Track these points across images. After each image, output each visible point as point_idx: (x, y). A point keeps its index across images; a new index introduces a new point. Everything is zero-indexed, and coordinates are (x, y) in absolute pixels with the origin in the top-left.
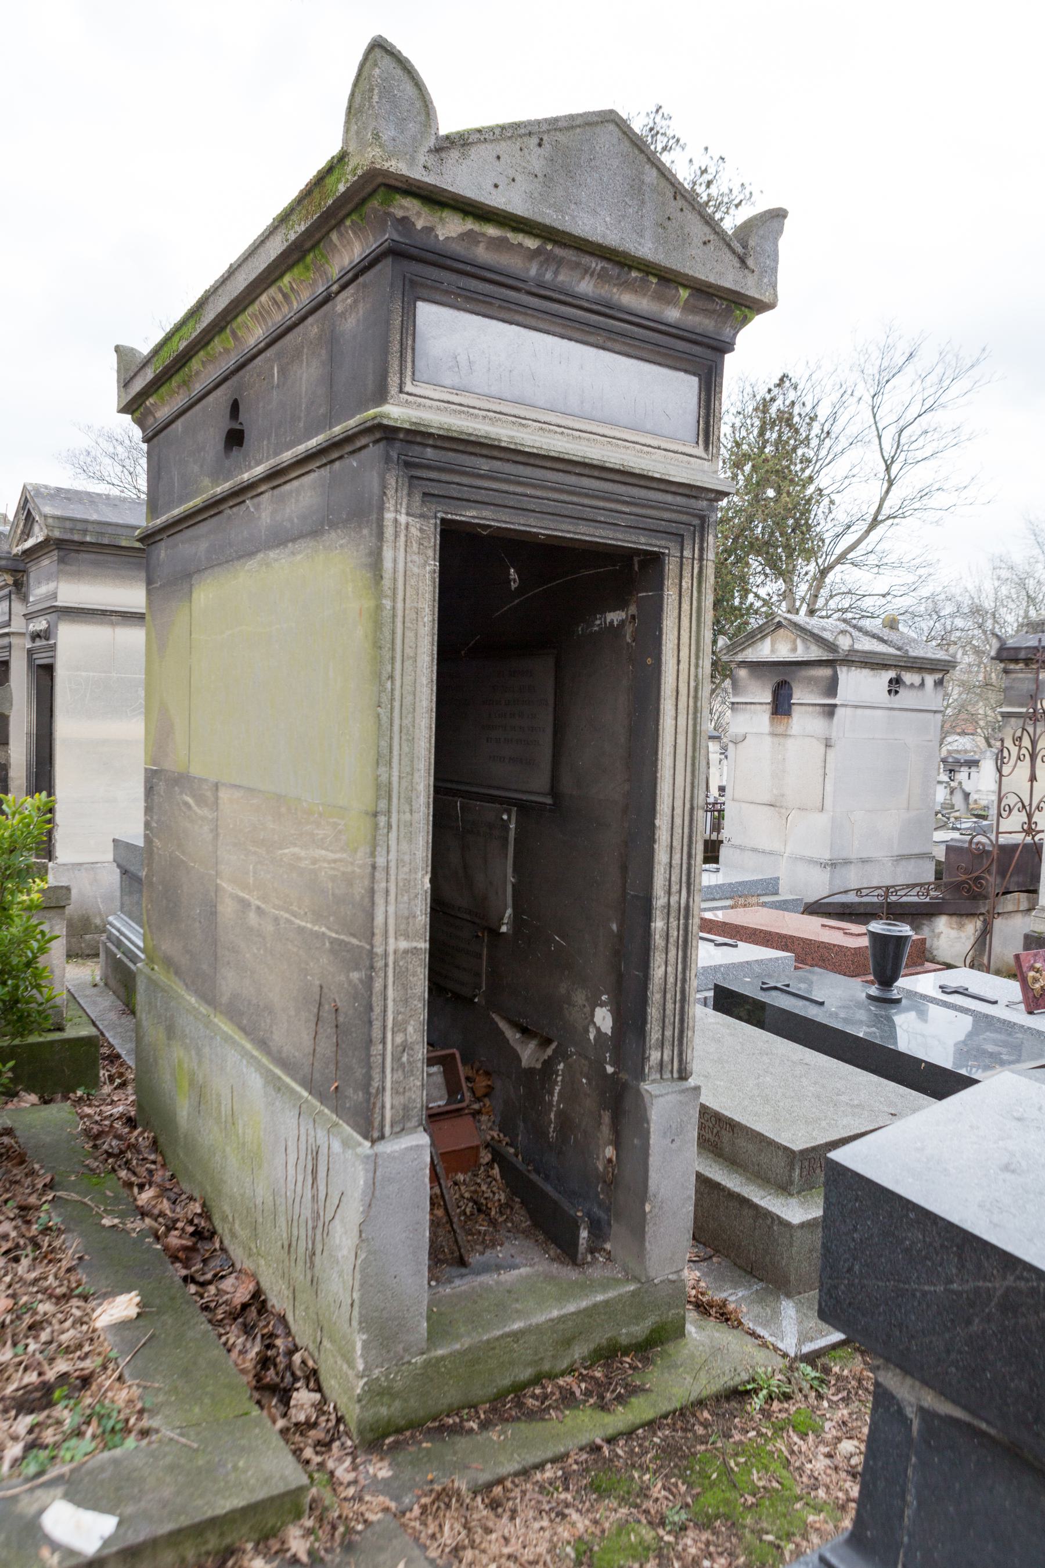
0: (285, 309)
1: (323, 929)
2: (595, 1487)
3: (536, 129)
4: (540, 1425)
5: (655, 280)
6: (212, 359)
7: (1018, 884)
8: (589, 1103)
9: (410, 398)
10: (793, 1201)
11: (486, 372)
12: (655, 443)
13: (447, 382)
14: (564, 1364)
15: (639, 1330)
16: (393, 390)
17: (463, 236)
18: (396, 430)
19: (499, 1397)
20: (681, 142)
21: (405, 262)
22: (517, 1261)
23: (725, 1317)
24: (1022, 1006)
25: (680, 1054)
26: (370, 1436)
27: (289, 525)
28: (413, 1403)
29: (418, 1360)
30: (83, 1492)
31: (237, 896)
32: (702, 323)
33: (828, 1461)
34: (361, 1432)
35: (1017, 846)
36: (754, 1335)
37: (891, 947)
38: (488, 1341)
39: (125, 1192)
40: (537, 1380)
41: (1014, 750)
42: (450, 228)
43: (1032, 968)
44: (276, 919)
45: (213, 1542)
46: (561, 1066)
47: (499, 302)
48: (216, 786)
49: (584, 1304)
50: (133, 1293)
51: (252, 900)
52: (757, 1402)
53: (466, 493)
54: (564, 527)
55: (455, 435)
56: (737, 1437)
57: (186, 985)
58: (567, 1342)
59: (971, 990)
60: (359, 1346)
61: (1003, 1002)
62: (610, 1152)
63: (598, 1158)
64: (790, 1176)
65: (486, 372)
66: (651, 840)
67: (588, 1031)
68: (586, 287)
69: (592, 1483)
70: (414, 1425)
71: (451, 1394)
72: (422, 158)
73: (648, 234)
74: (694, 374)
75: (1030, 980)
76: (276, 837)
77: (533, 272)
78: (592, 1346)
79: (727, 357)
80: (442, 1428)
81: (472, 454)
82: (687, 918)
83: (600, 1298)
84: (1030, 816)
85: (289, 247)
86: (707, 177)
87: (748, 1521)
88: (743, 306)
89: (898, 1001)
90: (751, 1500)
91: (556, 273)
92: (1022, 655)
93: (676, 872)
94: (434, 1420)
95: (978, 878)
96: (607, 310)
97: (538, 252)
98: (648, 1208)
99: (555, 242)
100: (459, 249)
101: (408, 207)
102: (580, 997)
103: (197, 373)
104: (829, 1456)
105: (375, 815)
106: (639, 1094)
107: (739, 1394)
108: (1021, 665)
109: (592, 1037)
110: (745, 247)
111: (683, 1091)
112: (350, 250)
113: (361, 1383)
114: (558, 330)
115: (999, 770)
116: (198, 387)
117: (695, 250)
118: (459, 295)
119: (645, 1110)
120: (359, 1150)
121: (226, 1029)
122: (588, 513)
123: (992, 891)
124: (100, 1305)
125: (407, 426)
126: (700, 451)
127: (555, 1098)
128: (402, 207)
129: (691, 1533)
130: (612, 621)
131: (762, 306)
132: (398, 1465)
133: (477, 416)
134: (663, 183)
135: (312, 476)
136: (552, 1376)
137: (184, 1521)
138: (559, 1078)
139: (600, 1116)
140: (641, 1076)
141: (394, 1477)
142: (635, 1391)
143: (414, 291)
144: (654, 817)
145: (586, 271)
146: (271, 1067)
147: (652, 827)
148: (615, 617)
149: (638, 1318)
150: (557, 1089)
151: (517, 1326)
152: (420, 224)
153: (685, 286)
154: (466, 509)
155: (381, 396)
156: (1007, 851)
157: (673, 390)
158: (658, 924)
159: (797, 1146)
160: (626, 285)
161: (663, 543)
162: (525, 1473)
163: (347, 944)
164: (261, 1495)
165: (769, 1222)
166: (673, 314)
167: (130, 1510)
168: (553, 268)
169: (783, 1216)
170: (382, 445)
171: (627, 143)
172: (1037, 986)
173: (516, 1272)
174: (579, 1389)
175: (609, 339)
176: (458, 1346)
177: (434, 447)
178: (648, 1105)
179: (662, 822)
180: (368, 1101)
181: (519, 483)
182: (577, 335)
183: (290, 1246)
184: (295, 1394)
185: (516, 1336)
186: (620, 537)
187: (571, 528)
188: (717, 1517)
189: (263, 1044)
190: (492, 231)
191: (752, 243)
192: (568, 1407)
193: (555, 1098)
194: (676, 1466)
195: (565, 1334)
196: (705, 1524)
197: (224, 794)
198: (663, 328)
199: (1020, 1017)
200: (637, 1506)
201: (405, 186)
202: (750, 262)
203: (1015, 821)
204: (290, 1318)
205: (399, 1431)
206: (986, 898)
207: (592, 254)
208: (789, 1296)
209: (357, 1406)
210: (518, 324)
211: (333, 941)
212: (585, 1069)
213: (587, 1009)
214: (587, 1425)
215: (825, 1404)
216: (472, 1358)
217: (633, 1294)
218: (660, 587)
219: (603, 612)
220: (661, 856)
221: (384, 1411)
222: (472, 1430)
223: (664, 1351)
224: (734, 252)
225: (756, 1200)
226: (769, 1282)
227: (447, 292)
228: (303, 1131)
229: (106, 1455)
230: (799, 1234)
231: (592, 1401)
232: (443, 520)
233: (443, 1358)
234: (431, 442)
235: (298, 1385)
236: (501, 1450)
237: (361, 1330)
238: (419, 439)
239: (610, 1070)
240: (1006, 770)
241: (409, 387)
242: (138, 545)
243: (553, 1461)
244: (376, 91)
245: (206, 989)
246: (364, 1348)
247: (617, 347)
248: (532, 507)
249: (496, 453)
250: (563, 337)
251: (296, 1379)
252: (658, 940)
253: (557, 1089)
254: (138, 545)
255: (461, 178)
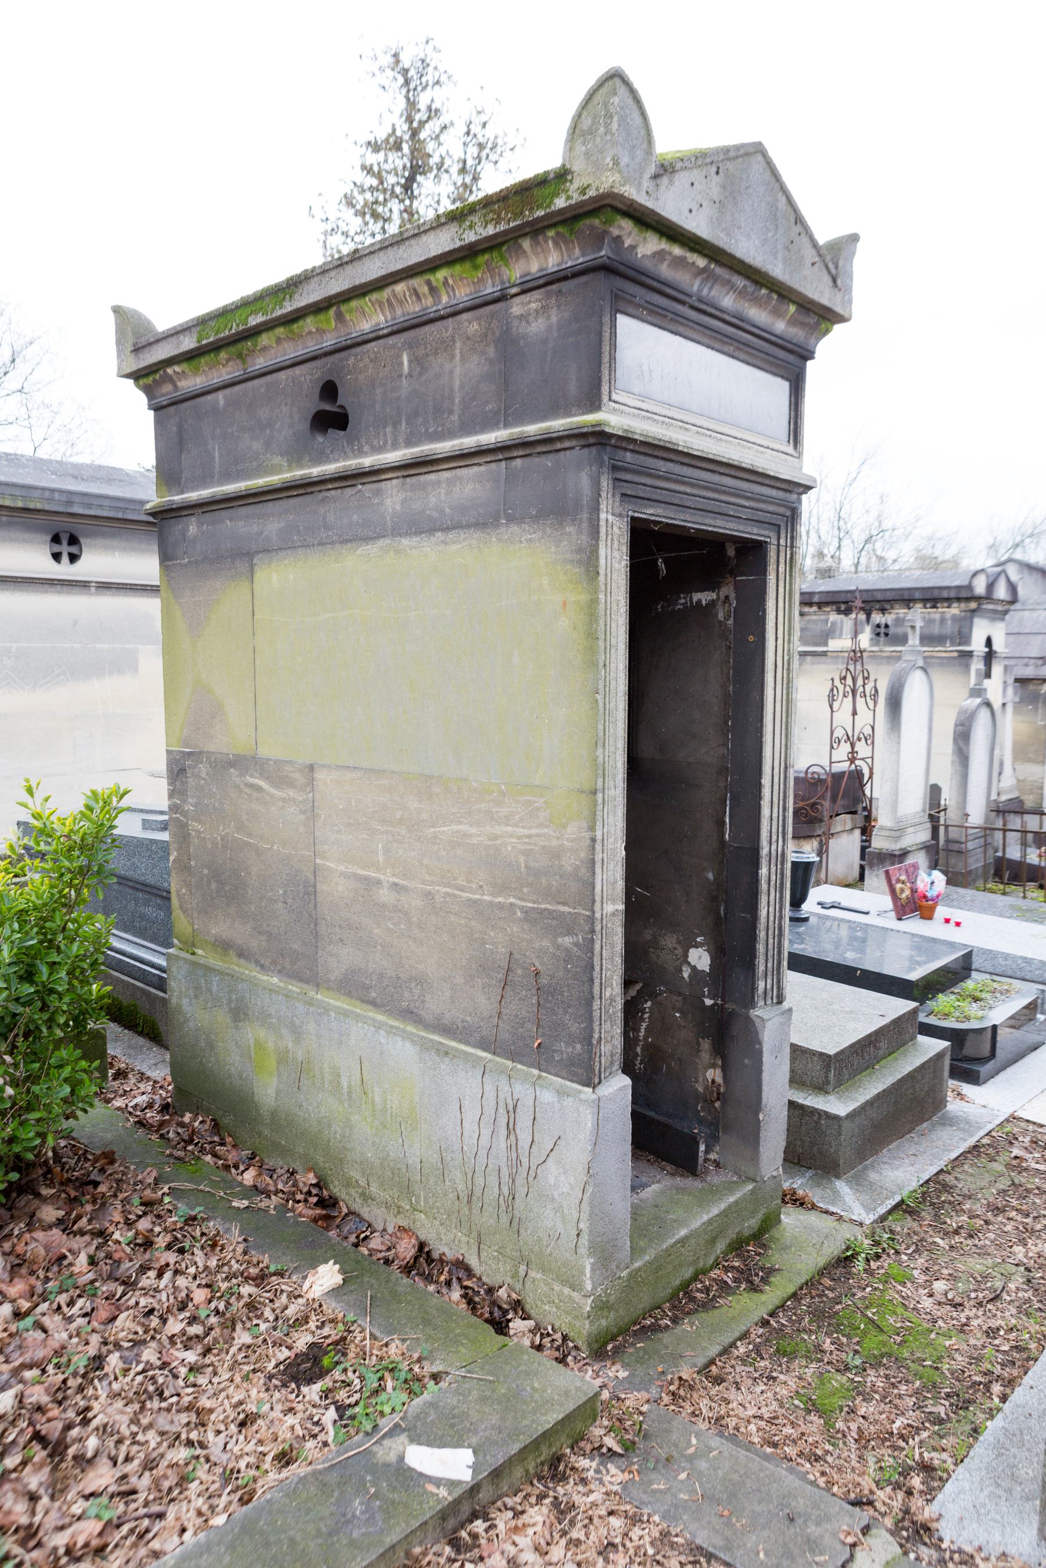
0: (429, 301)
1: (512, 900)
2: (780, 1352)
3: (715, 158)
4: (716, 1312)
5: (775, 297)
6: (293, 338)
7: (844, 807)
8: (685, 1034)
9: (617, 406)
10: (831, 1098)
11: (669, 382)
12: (765, 443)
13: (636, 390)
14: (711, 1261)
15: (753, 1223)
16: (605, 398)
17: (655, 254)
18: (611, 436)
19: (673, 1297)
20: (454, 78)
21: (612, 277)
22: (644, 1180)
23: (800, 1203)
24: (893, 914)
25: (779, 982)
26: (595, 1346)
27: (435, 514)
28: (622, 1312)
29: (624, 1274)
30: (441, 1433)
31: (355, 875)
32: (796, 334)
33: (931, 1300)
34: (589, 1344)
35: (843, 773)
36: (826, 1212)
37: (801, 872)
38: (667, 1250)
39: (224, 1174)
40: (695, 1278)
41: (841, 687)
42: (648, 247)
43: (898, 881)
44: (428, 895)
45: (545, 1453)
46: (649, 1004)
47: (670, 316)
48: (311, 768)
49: (723, 1206)
50: (331, 1262)
51: (382, 877)
52: (860, 1265)
53: (647, 492)
54: (707, 521)
55: (650, 440)
56: (860, 1294)
57: (262, 967)
58: (713, 1241)
59: (843, 905)
60: (588, 1269)
61: (873, 912)
62: (714, 1074)
63: (697, 1081)
64: (827, 1077)
65: (669, 382)
66: (759, 797)
67: (681, 971)
68: (728, 301)
69: (778, 1350)
70: (624, 1331)
71: (645, 1300)
72: (646, 184)
73: (780, 256)
74: (787, 379)
75: (898, 891)
76: (424, 816)
77: (695, 288)
78: (728, 1241)
79: (809, 363)
80: (644, 1329)
81: (657, 457)
82: (782, 863)
83: (732, 1199)
84: (853, 745)
85: (461, 248)
86: (483, 118)
87: (906, 1355)
88: (823, 317)
89: (806, 920)
90: (899, 1339)
91: (710, 289)
92: (816, 599)
93: (775, 823)
94: (635, 1324)
95: (813, 805)
96: (739, 323)
97: (704, 270)
98: (761, 1117)
99: (717, 262)
100: (649, 265)
101: (624, 228)
102: (670, 941)
103: (265, 349)
104: (931, 1296)
105: (594, 792)
106: (749, 1020)
107: (845, 1260)
108: (815, 608)
109: (686, 975)
110: (837, 268)
111: (782, 1014)
112: (549, 257)
113: (590, 1301)
114: (706, 340)
115: (831, 707)
116: (260, 363)
117: (807, 271)
118: (645, 308)
119: (757, 1032)
120: (582, 1096)
121: (338, 1004)
122: (724, 508)
123: (826, 814)
124: (305, 1278)
125: (620, 433)
126: (790, 449)
127: (642, 1034)
128: (620, 227)
129: (871, 1372)
130: (700, 601)
131: (841, 319)
132: (628, 1365)
133: (686, 429)
134: (790, 210)
135: (475, 469)
136: (705, 1272)
137: (525, 1440)
138: (646, 1016)
139: (698, 1044)
140: (751, 1003)
141: (632, 1375)
142: (771, 1271)
143: (620, 304)
144: (760, 777)
145: (732, 287)
146: (423, 1034)
147: (759, 786)
148: (704, 597)
149: (754, 1212)
150: (644, 1025)
151: (683, 1232)
152: (628, 242)
153: (794, 302)
154: (646, 507)
155: (594, 403)
156: (838, 777)
157: (759, 391)
158: (763, 871)
159: (832, 1051)
160: (756, 301)
161: (766, 533)
162: (725, 1351)
163: (551, 912)
164: (570, 1406)
165: (816, 1118)
166: (780, 326)
167: (474, 1440)
168: (709, 285)
169: (829, 1110)
170: (594, 450)
171: (768, 173)
172: (904, 896)
173: (649, 1189)
174: (729, 1277)
175: (738, 349)
176: (647, 1258)
177: (632, 451)
178: (759, 1028)
179: (766, 781)
180: (590, 1052)
181: (684, 483)
182: (717, 345)
183: (470, 1197)
184: (511, 1324)
185: (683, 1241)
186: (741, 528)
187: (712, 522)
188: (882, 1356)
189: (410, 1015)
190: (677, 251)
191: (841, 264)
192: (728, 1294)
193: (642, 1034)
194: (829, 1325)
195: (711, 1233)
196: (877, 1365)
197: (320, 775)
198: (773, 338)
199: (890, 922)
200: (821, 1360)
201: (625, 208)
202: (839, 282)
203: (842, 752)
204: (473, 1261)
205: (613, 1338)
206: (821, 821)
207: (739, 273)
208: (838, 1177)
209: (587, 1322)
210: (681, 335)
211: (526, 911)
212: (679, 1005)
213: (679, 951)
214: (747, 1308)
215: (904, 1257)
216: (656, 1267)
217: (753, 1191)
218: (764, 572)
219: (689, 591)
220: (765, 812)
221: (604, 1322)
222: (667, 1326)
223: (772, 1237)
224: (829, 272)
225: (801, 1101)
226: (819, 1168)
227: (638, 306)
228: (487, 1087)
229: (418, 1401)
230: (845, 1124)
231: (743, 1286)
232: (633, 519)
233: (639, 1269)
234: (631, 447)
235: (510, 1316)
236: (696, 1339)
237: (589, 1255)
238: (624, 445)
239: (709, 1002)
240: (836, 705)
241: (614, 397)
242: (151, 519)
243: (740, 1339)
244: (615, 119)
245: (305, 970)
246: (593, 1270)
247: (742, 356)
248: (689, 504)
249: (672, 456)
250: (708, 346)
251: (506, 1312)
252: (764, 886)
253: (644, 1025)
254: (151, 519)
255: (673, 204)
